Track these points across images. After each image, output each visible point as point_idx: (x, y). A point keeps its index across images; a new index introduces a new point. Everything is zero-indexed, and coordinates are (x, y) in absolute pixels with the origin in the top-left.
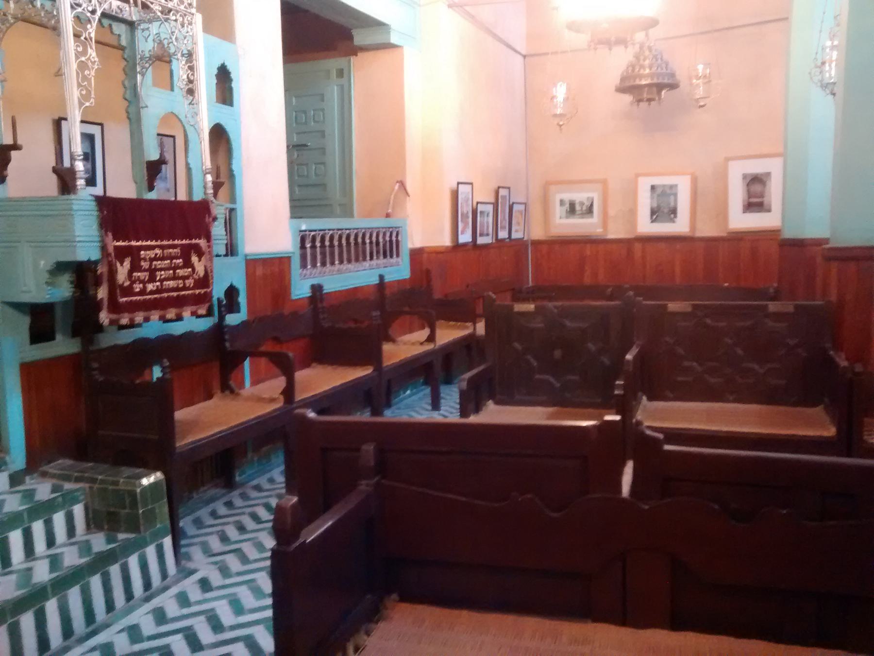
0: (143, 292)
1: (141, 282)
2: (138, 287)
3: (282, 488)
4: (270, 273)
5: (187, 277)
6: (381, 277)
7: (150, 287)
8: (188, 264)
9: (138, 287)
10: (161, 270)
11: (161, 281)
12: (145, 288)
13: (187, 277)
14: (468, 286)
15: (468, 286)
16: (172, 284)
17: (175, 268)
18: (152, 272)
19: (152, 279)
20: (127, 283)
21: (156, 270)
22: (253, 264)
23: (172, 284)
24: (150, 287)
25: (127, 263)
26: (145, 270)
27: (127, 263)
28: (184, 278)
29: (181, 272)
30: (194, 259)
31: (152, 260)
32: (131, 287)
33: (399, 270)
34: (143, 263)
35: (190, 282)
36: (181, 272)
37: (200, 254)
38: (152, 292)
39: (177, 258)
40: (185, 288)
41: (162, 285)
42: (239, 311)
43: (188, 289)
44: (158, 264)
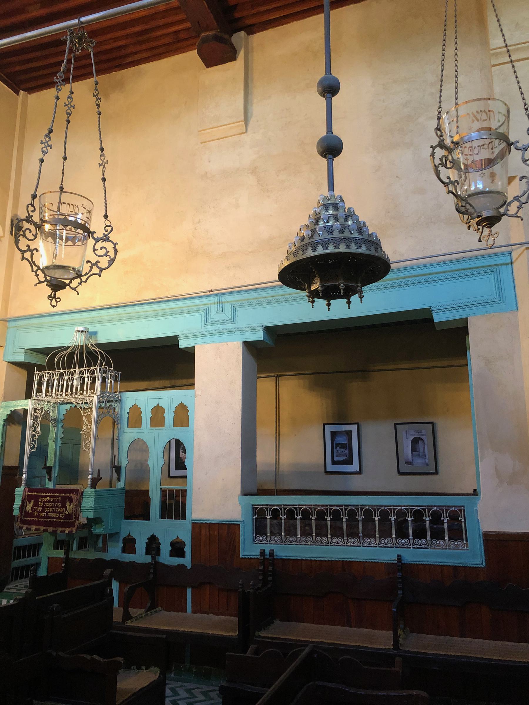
0: (38, 516)
1: (37, 511)
2: (35, 514)
3: (168, 684)
4: (218, 536)
5: (62, 513)
6: (399, 558)
7: (42, 515)
8: (64, 506)
9: (35, 514)
10: (48, 507)
11: (47, 512)
12: (39, 515)
13: (62, 513)
14: (223, 480)
15: (223, 480)
16: (54, 515)
17: (56, 508)
18: (44, 508)
19: (43, 511)
20: (30, 512)
21: (46, 507)
22: (198, 527)
23: (54, 515)
24: (42, 515)
25: (32, 503)
26: (40, 507)
27: (32, 503)
28: (60, 513)
29: (59, 510)
30: (68, 503)
31: (44, 502)
32: (32, 513)
33: (470, 554)
34: (40, 503)
35: (62, 516)
36: (59, 510)
37: (71, 501)
38: (42, 517)
39: (58, 502)
40: (59, 518)
41: (47, 514)
42: (171, 555)
43: (61, 519)
44: (48, 505)
